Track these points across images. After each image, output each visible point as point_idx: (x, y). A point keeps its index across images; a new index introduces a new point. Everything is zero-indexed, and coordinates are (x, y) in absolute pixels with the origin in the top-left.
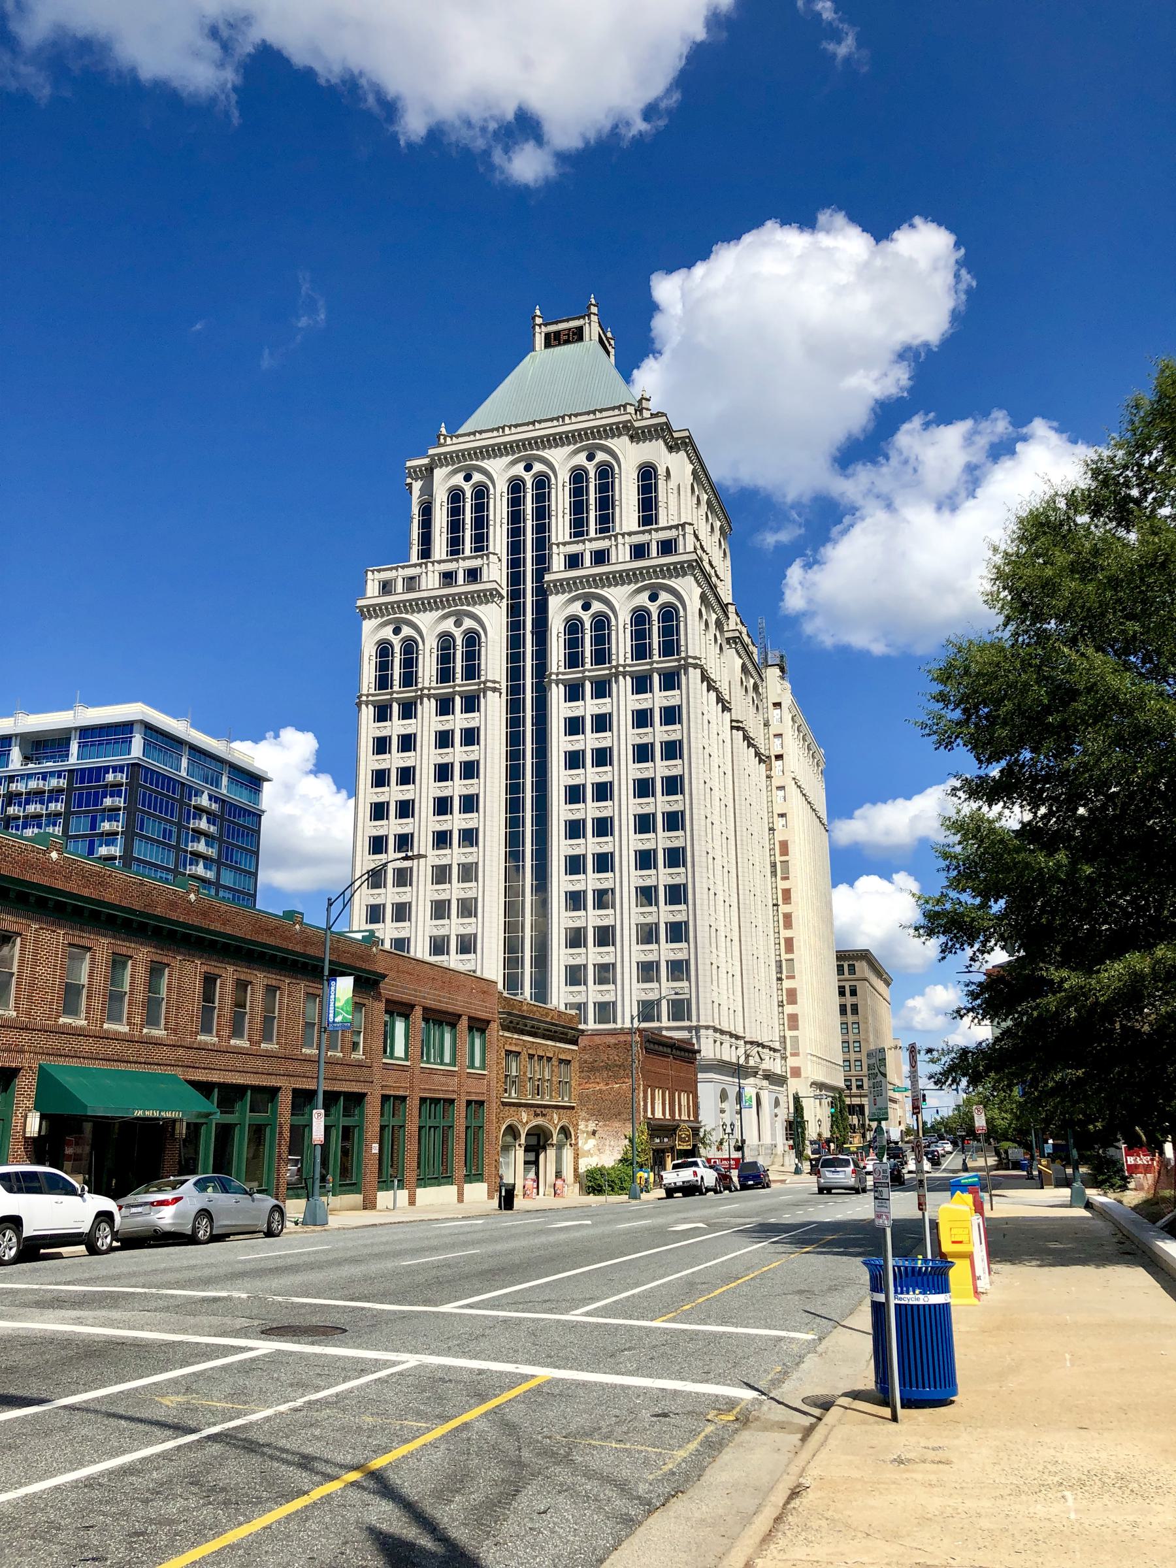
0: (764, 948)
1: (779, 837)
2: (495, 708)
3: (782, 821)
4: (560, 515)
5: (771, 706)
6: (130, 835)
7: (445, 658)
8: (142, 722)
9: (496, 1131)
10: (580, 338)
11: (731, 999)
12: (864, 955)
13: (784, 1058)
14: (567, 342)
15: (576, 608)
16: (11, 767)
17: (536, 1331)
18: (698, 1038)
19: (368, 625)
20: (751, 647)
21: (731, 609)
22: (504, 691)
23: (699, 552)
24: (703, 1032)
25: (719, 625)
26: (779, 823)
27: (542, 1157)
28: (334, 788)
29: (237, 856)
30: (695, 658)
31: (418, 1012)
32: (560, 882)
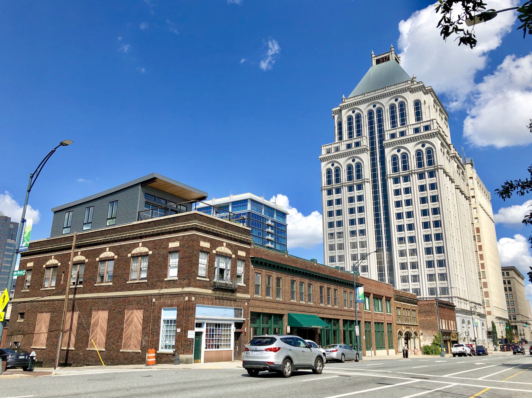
0: (474, 268)
2: (368, 188)
3: (476, 220)
4: (387, 121)
5: (469, 179)
7: (350, 173)
8: (250, 199)
9: (396, 333)
10: (389, 59)
11: (463, 287)
12: (513, 269)
13: (484, 308)
14: (383, 62)
15: (395, 152)
17: (475, 381)
18: (452, 301)
19: (323, 164)
20: (460, 158)
21: (452, 146)
23: (439, 128)
24: (454, 299)
25: (448, 152)
26: (475, 221)
27: (409, 341)
28: (297, 212)
29: (280, 239)
30: (441, 166)
31: (372, 296)
32: (396, 247)
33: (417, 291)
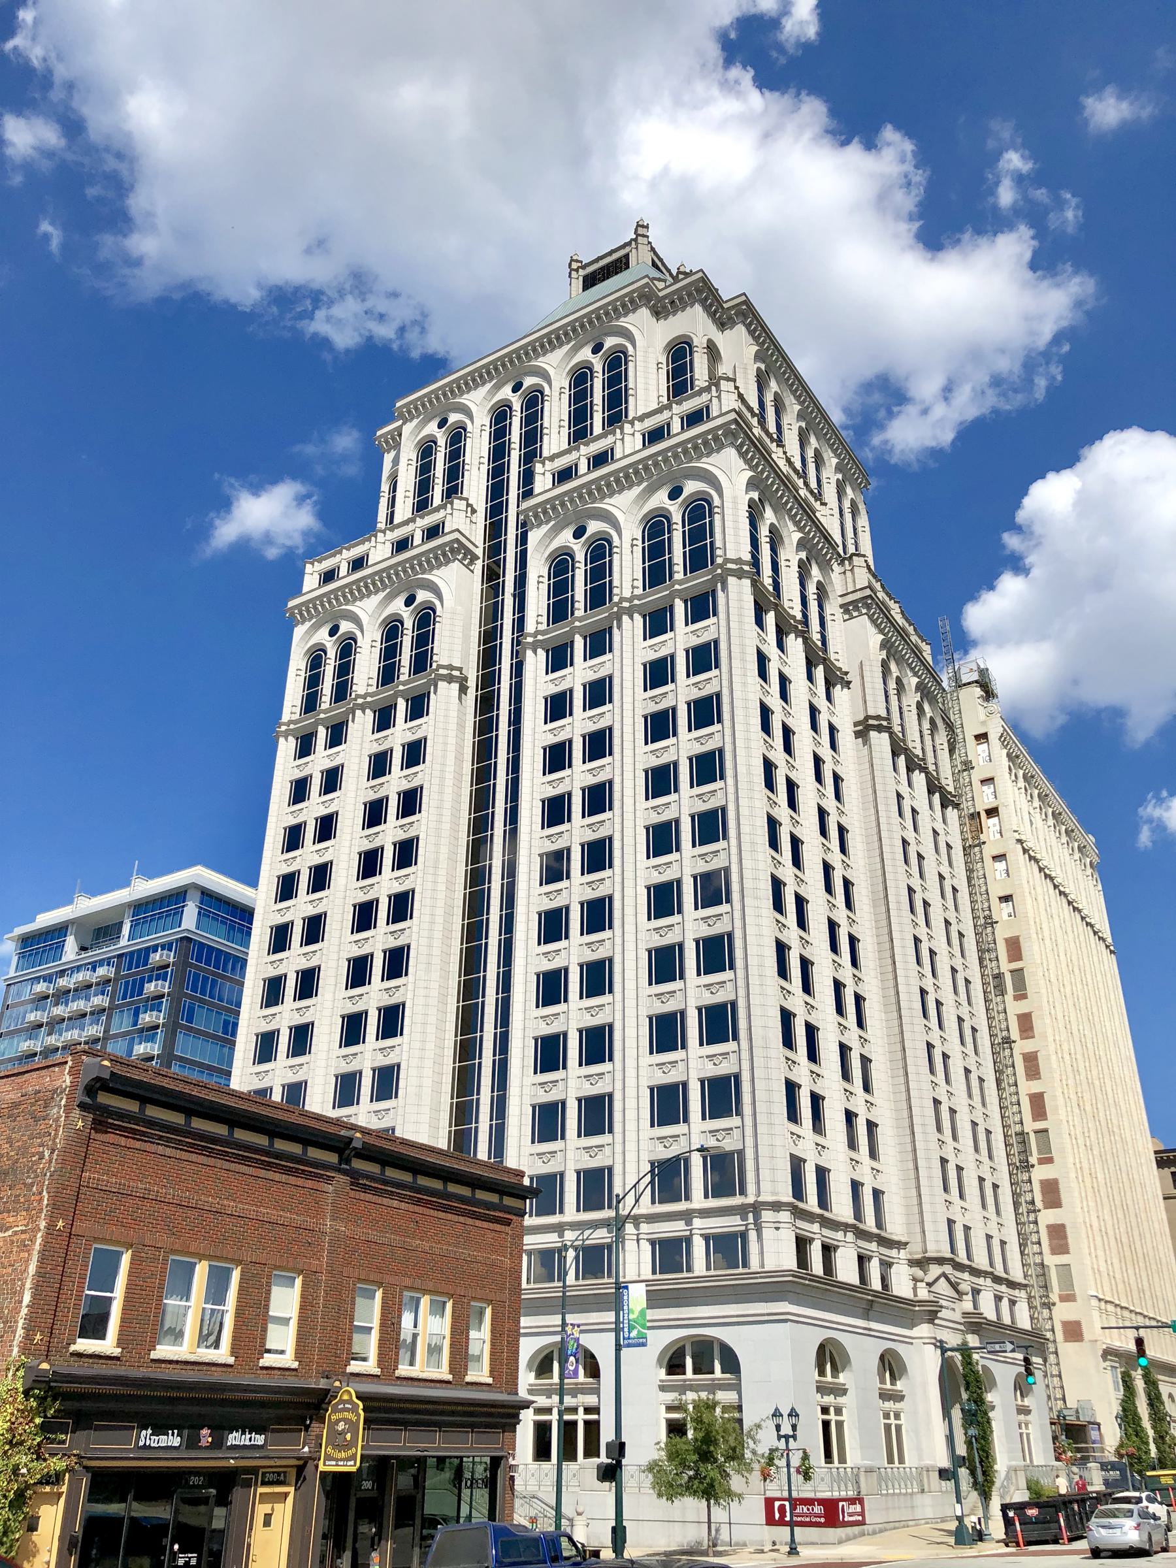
1: (1002, 933)
3: (1006, 908)
5: (970, 741)
6: (172, 1028)
8: (195, 886)
16: (64, 960)
22: (472, 683)
24: (767, 1215)
26: (1001, 912)
33: (296, 1091)
